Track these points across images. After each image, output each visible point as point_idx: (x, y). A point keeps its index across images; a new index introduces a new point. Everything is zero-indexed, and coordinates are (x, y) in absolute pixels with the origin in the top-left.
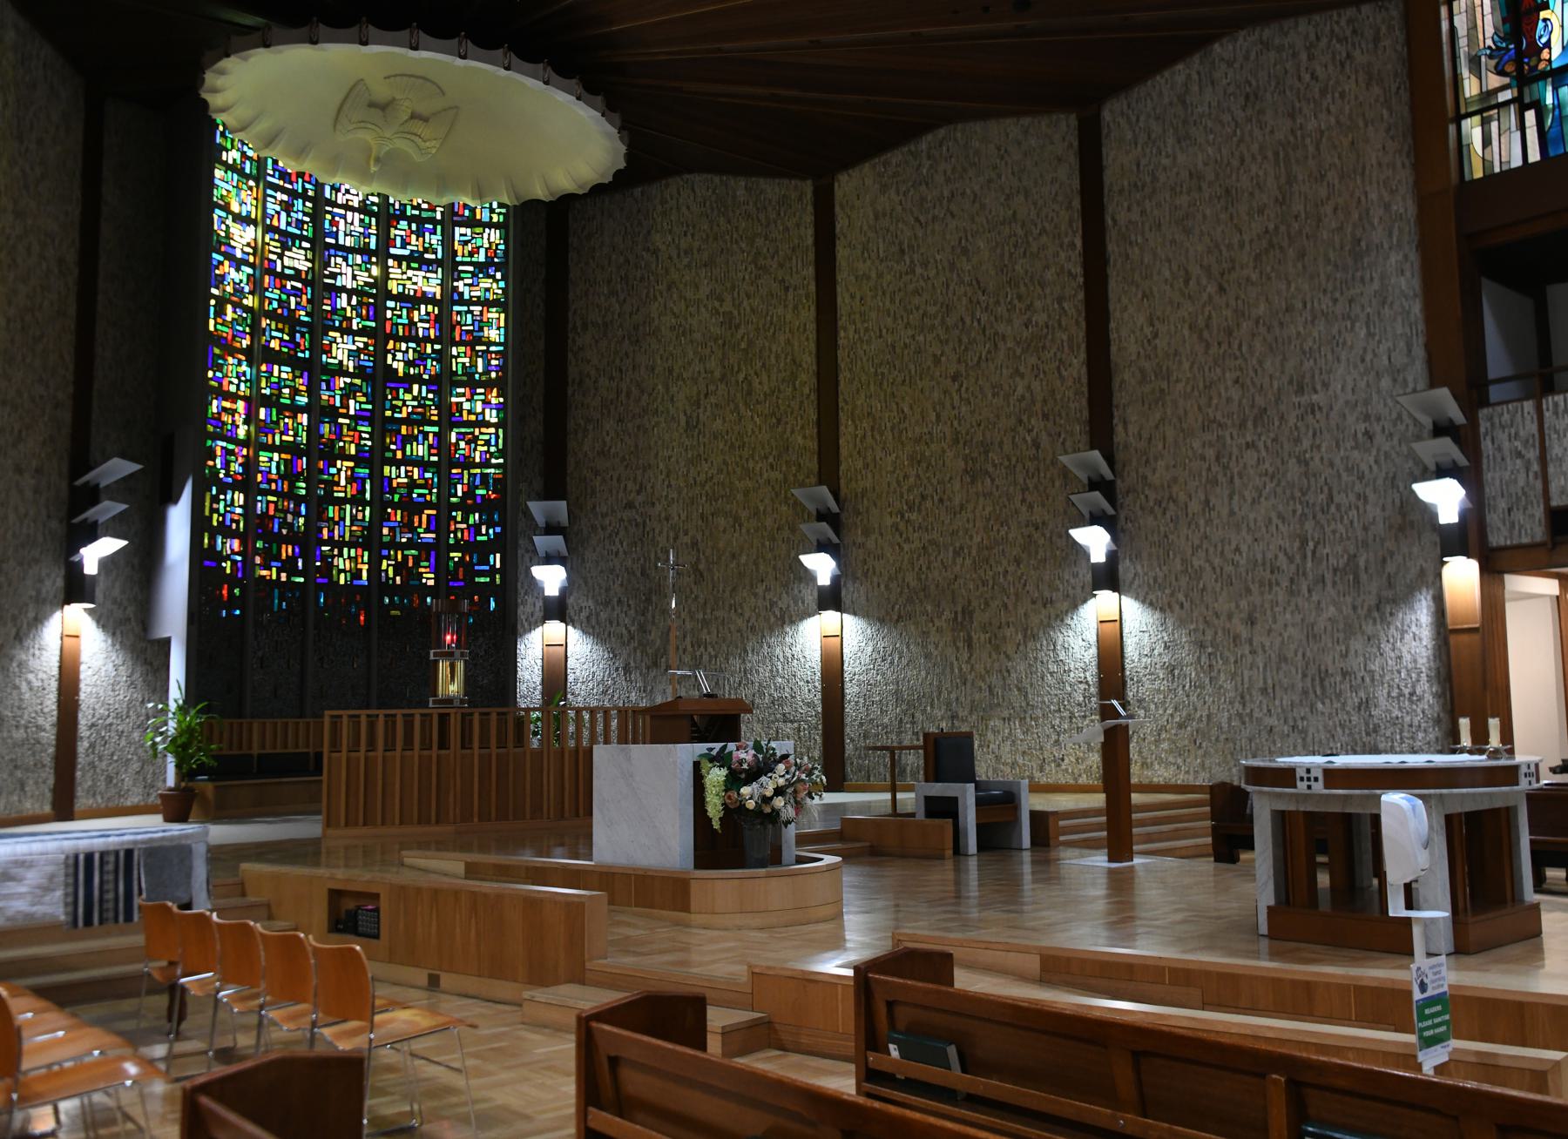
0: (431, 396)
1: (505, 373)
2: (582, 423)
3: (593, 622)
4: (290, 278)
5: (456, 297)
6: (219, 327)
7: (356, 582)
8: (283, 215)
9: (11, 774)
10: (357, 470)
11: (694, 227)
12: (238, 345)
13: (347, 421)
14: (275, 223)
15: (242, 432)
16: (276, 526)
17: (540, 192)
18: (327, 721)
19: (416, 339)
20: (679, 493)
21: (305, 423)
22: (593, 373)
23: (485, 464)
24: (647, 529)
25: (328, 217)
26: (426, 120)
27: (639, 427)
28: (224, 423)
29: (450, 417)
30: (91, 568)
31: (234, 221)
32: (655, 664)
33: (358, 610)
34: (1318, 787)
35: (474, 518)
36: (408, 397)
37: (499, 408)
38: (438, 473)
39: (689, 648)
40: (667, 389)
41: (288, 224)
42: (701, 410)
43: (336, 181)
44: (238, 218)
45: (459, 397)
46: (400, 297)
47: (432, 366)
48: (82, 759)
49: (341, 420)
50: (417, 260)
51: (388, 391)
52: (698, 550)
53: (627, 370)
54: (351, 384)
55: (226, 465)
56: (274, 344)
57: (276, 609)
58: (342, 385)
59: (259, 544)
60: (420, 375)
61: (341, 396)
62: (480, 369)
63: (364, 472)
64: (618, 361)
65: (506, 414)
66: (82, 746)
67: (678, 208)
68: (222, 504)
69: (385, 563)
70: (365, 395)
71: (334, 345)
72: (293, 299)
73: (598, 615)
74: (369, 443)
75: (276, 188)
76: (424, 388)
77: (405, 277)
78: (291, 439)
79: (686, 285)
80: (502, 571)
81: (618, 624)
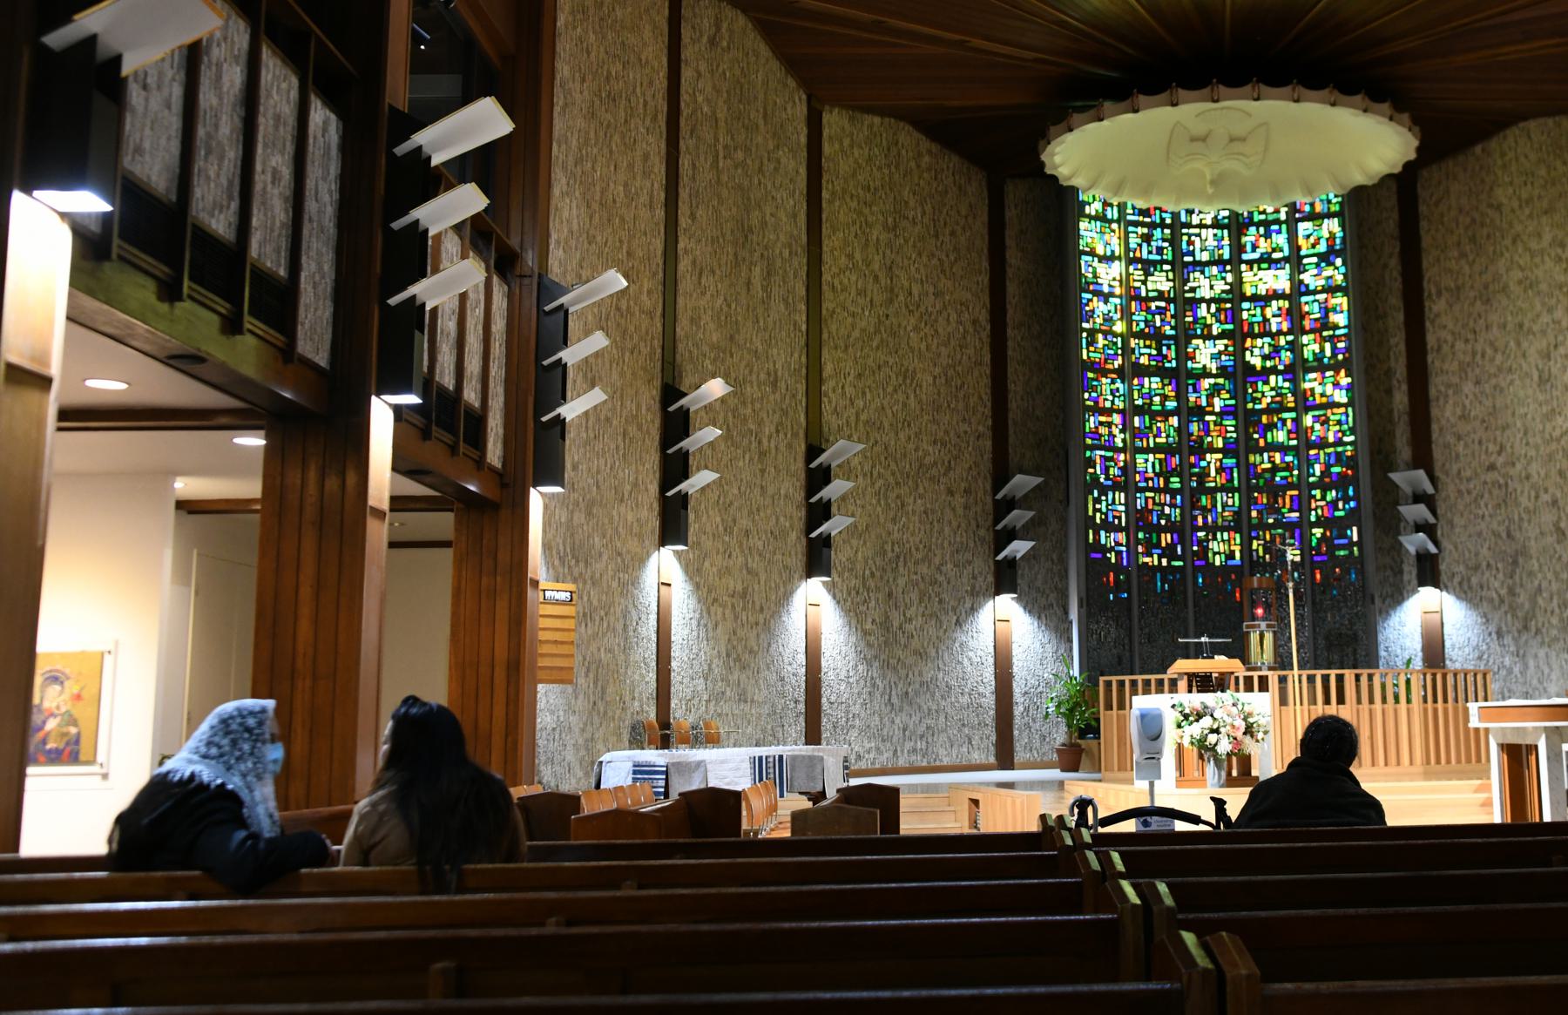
0: (1287, 384)
1: (1350, 353)
2: (1443, 389)
4: (1154, 299)
5: (1303, 289)
6: (1091, 355)
7: (1230, 562)
8: (1145, 245)
9: (960, 730)
10: (1225, 461)
11: (1533, 176)
12: (1110, 367)
13: (1213, 418)
14: (1138, 254)
15: (1119, 443)
16: (1155, 519)
17: (1360, 179)
18: (1101, 683)
19: (1272, 336)
20: (1538, 451)
21: (1176, 425)
22: (1449, 338)
23: (1339, 442)
24: (1510, 490)
25: (1185, 238)
26: (1243, 140)
27: (1495, 387)
28: (1101, 435)
29: (1304, 403)
31: (1100, 261)
32: (1526, 628)
33: (1234, 587)
35: (1331, 495)
36: (1266, 388)
37: (1349, 388)
38: (1297, 455)
39: (1557, 610)
40: (1518, 344)
41: (1150, 252)
42: (1552, 362)
43: (1190, 207)
44: (1104, 259)
45: (1311, 382)
46: (1255, 298)
47: (1286, 356)
48: (1017, 721)
49: (1208, 418)
50: (1267, 261)
51: (1248, 385)
52: (1559, 508)
53: (1481, 331)
54: (1216, 384)
55: (1106, 470)
56: (1144, 360)
57: (1159, 591)
58: (1207, 387)
59: (1141, 535)
60: (1275, 366)
61: (1207, 396)
62: (1328, 353)
63: (1230, 462)
64: (1471, 323)
65: (1353, 394)
66: (1018, 711)
67: (1517, 159)
68: (1104, 504)
70: (1228, 392)
71: (1197, 351)
72: (1158, 318)
73: (1469, 580)
74: (1234, 435)
75: (1136, 224)
76: (1280, 378)
77: (1257, 278)
78: (1164, 440)
79: (1529, 236)
80: (1360, 544)
81: (1489, 589)
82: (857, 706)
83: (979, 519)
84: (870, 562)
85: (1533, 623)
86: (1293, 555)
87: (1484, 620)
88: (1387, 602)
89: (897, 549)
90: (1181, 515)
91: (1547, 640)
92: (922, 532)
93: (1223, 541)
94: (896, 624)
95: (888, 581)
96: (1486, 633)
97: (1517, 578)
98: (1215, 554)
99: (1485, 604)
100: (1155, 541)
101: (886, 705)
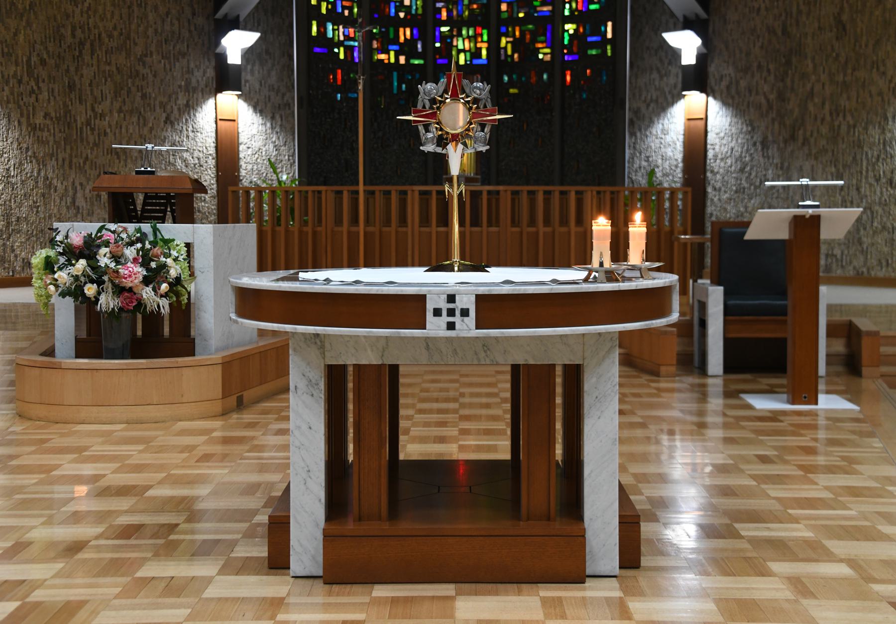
3: (733, 91)
7: (476, 62)
16: (393, 11)
18: (230, 194)
30: (234, 58)
32: (793, 138)
34: (467, 327)
39: (828, 118)
57: (395, 91)
69: (504, 41)
73: (737, 83)
81: (757, 93)
82: (24, 209)
83: (196, 6)
84: (37, 46)
85: (801, 132)
86: (544, 54)
87: (750, 129)
88: (651, 108)
89: (79, 32)
90: (423, 7)
91: (814, 151)
92: (117, 17)
93: (469, 37)
94: (81, 120)
95: (68, 71)
96: (751, 143)
97: (788, 81)
98: (459, 51)
99: (752, 110)
100: (392, 36)
101: (68, 208)
